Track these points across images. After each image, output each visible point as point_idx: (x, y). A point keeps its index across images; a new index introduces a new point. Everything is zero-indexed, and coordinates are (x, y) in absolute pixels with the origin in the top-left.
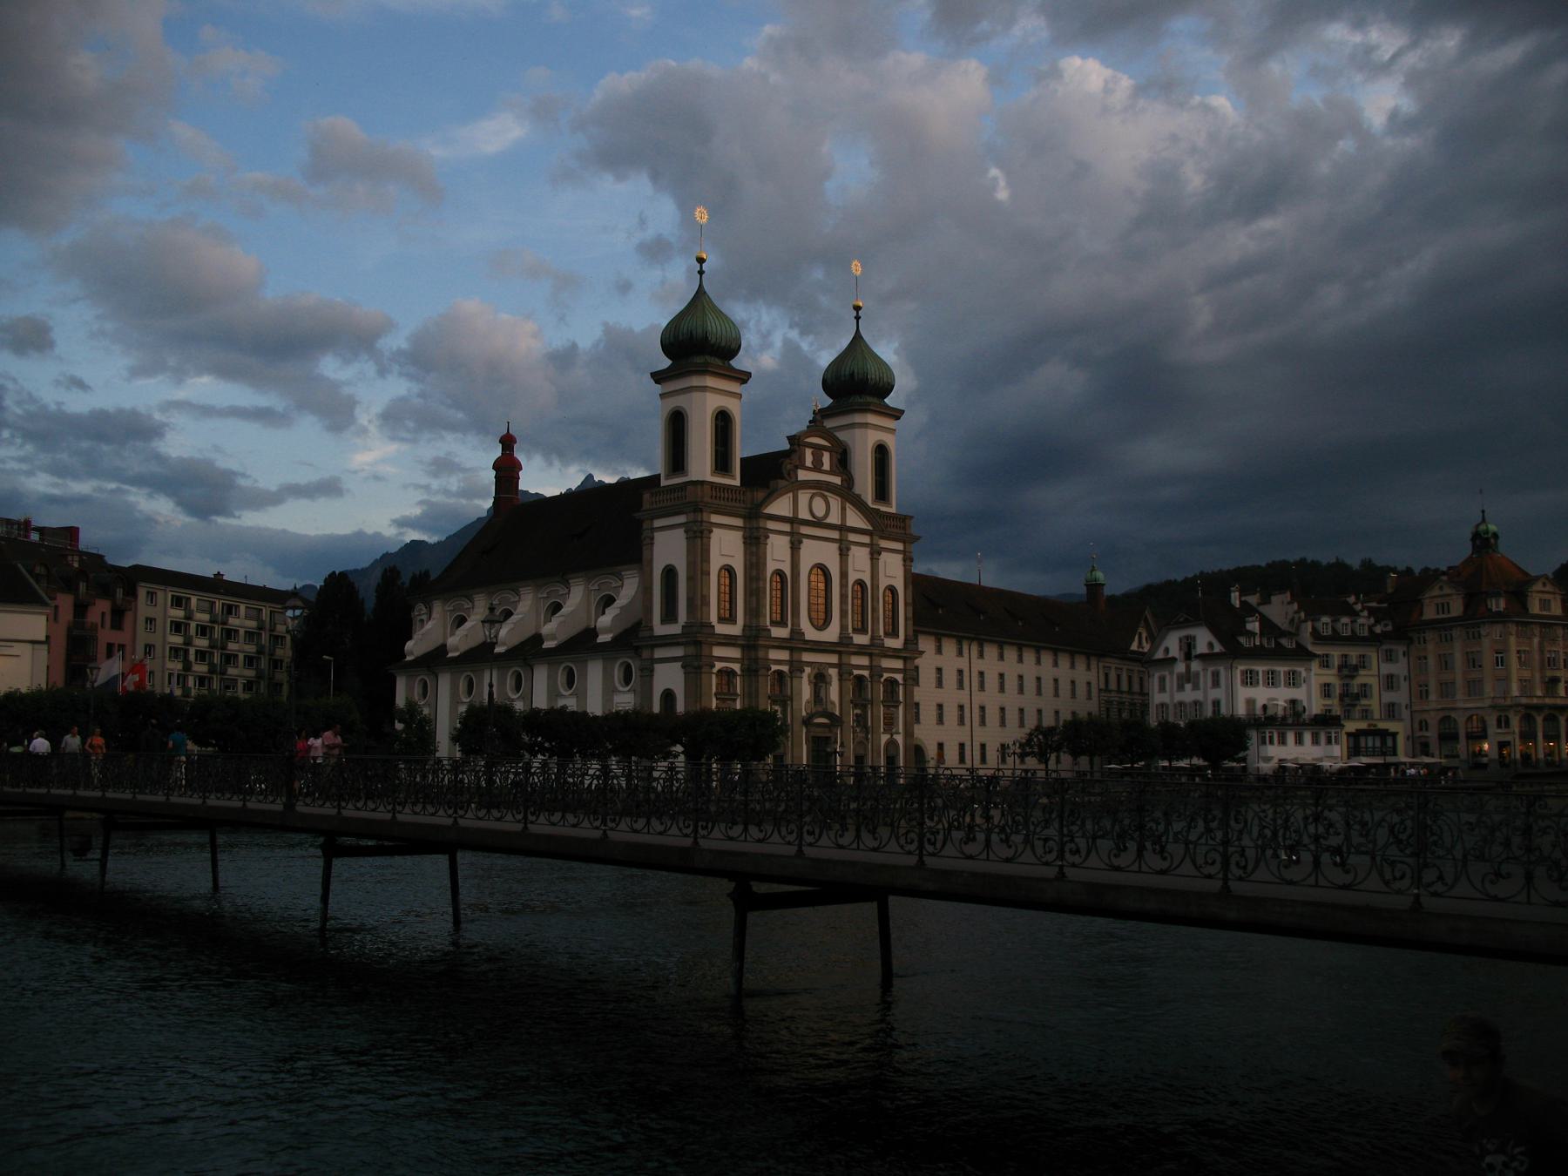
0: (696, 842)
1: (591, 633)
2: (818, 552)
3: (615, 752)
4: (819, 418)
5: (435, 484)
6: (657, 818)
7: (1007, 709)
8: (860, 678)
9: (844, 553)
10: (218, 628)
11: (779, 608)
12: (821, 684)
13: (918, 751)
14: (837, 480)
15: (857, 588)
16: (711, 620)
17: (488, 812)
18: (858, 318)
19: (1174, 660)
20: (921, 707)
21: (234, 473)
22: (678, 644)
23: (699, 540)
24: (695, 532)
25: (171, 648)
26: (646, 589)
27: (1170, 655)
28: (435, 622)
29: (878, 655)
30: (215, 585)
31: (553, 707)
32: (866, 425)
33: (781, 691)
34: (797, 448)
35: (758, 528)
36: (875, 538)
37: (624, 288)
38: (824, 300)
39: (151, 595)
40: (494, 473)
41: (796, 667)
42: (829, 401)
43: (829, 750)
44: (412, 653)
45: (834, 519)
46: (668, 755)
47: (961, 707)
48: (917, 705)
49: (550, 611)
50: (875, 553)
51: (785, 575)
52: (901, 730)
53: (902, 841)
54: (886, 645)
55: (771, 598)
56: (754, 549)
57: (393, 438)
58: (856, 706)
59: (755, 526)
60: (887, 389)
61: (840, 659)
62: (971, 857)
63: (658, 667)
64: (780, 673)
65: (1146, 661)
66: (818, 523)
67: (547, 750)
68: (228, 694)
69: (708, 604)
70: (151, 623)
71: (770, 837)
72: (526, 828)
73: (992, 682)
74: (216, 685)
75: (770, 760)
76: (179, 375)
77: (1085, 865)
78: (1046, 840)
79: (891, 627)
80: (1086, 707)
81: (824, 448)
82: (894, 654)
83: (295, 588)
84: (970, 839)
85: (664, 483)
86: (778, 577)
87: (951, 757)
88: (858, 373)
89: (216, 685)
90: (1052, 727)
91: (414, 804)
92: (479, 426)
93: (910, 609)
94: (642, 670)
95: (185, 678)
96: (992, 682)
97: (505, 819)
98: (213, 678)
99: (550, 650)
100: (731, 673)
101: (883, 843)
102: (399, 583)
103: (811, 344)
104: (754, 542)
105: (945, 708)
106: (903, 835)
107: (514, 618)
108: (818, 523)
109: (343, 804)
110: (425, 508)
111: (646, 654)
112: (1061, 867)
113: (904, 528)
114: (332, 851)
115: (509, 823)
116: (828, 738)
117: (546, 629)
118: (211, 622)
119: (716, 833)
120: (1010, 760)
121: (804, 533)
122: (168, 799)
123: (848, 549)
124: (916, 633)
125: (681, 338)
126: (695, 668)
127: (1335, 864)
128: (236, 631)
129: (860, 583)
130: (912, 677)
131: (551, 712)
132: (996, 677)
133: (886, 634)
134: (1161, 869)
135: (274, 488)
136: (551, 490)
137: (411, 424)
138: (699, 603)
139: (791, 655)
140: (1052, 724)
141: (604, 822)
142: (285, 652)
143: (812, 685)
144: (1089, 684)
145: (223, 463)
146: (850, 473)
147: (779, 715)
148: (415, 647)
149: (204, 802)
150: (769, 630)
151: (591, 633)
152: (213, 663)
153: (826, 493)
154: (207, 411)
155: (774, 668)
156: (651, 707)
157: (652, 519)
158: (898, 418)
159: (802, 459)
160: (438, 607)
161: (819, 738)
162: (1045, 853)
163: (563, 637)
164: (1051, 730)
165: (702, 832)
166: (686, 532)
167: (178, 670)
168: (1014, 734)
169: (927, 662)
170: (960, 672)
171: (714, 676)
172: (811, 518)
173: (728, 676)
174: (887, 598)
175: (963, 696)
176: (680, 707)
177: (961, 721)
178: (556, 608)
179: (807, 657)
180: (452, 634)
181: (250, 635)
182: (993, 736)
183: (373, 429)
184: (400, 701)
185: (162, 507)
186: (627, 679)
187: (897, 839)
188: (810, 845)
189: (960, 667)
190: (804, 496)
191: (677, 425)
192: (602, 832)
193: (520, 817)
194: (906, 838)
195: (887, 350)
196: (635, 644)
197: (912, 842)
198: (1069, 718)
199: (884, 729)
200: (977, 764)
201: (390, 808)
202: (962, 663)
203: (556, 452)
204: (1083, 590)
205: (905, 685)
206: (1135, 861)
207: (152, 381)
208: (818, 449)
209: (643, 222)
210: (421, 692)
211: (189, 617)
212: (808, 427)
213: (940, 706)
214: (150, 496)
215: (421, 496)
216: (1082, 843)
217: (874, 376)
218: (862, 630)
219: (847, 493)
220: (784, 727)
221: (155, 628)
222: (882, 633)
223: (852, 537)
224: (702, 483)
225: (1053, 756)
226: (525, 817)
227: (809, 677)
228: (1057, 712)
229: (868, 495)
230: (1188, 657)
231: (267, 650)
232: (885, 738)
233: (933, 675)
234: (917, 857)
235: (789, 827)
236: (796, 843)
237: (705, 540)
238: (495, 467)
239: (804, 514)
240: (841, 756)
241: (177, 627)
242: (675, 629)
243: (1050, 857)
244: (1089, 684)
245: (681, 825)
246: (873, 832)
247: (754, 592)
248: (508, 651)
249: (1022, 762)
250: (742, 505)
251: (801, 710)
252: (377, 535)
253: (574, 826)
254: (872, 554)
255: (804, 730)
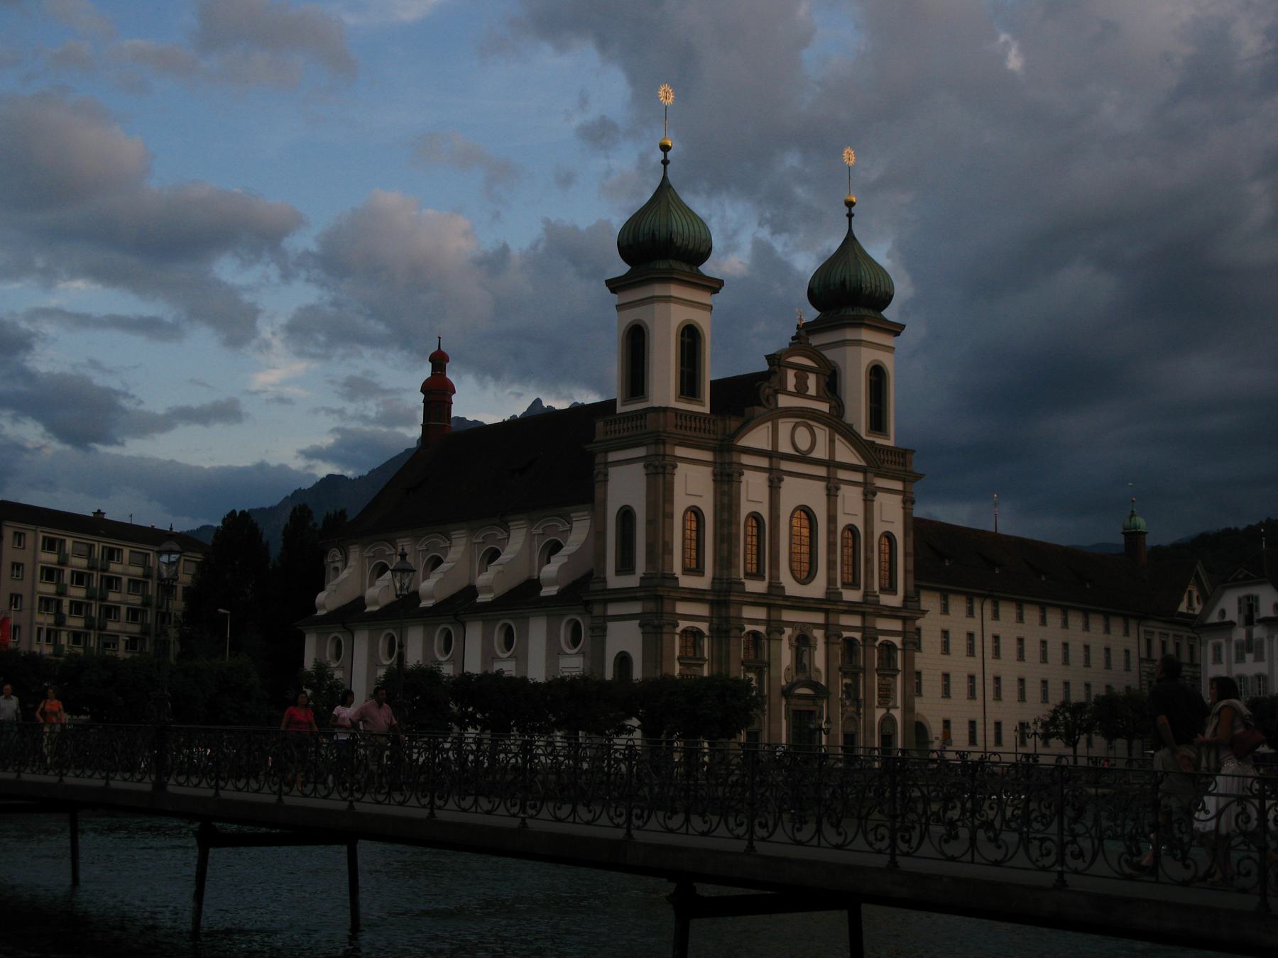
0: (629, 834)
1: (533, 585)
2: (810, 493)
3: (558, 726)
4: (803, 333)
5: (351, 408)
6: (584, 805)
7: (1026, 680)
8: (850, 641)
9: (832, 494)
10: (96, 576)
11: (754, 557)
12: (803, 649)
13: (920, 730)
14: (824, 407)
15: (885, 541)
16: (675, 571)
17: (188, 779)
18: (850, 216)
19: (1231, 624)
20: (924, 677)
21: (116, 393)
22: (635, 599)
23: (661, 476)
24: (656, 467)
25: (41, 599)
26: (599, 534)
27: (1227, 619)
28: (351, 570)
29: (870, 614)
30: (95, 525)
31: (486, 672)
32: (859, 343)
33: (756, 657)
34: (777, 369)
35: (731, 463)
36: (870, 475)
37: (566, 180)
38: (800, 192)
39: (19, 536)
40: (422, 396)
41: (775, 627)
42: (626, 268)
43: (812, 726)
44: (323, 607)
45: (821, 453)
46: (622, 730)
47: (972, 678)
48: (919, 674)
49: (486, 560)
50: (869, 494)
51: (858, 531)
52: (899, 704)
53: (871, 837)
54: (881, 603)
55: (746, 544)
56: (726, 488)
57: (300, 354)
58: (845, 675)
59: (661, 452)
60: (886, 300)
61: (827, 618)
62: (952, 859)
63: (611, 626)
64: (755, 635)
65: (1196, 625)
66: (802, 458)
67: (479, 722)
68: (107, 653)
69: (671, 552)
70: (18, 569)
71: (851, 842)
72: (432, 814)
73: (1009, 648)
74: (93, 642)
75: (742, 738)
76: (49, 277)
77: (915, 854)
78: (1042, 840)
79: (887, 581)
80: (1124, 679)
81: (811, 370)
82: (892, 613)
83: (171, 529)
84: (952, 836)
85: (620, 409)
86: (754, 522)
87: (960, 738)
88: (850, 281)
89: (93, 642)
90: (1082, 703)
91: (304, 784)
92: (403, 338)
93: (911, 560)
94: (592, 629)
95: (57, 633)
96: (1009, 648)
97: (598, 822)
98: (90, 634)
99: (486, 606)
100: (697, 634)
101: (848, 840)
102: (311, 524)
103: (785, 245)
104: (726, 479)
105: (952, 679)
106: (871, 830)
107: (444, 567)
108: (802, 458)
109: (222, 784)
110: (338, 437)
111: (597, 610)
112: (1061, 874)
113: (904, 465)
114: (209, 839)
115: (415, 809)
116: (812, 712)
117: (482, 580)
118: (89, 568)
119: (653, 824)
120: (1030, 742)
121: (785, 469)
122: (19, 776)
123: (838, 489)
124: (918, 589)
125: (641, 239)
126: (655, 627)
127: (989, 839)
128: (119, 579)
129: (851, 529)
130: (913, 641)
131: (485, 676)
132: (964, 637)
133: (882, 590)
134: (952, 856)
135: (161, 411)
136: (490, 418)
137: (321, 338)
138: (661, 550)
139: (769, 614)
140: (1082, 699)
141: (523, 809)
142: (177, 605)
143: (794, 649)
144: (1127, 652)
145: (100, 380)
146: (841, 399)
147: (754, 683)
148: (327, 600)
149: (61, 780)
150: (743, 584)
151: (533, 585)
152: (91, 617)
153: (811, 423)
154: (82, 321)
155: (748, 628)
156: (603, 674)
157: (607, 452)
158: (897, 334)
159: (783, 382)
160: (355, 554)
161: (800, 711)
162: (1042, 855)
163: (501, 590)
164: (1080, 707)
165: (636, 822)
166: (646, 467)
167: (48, 624)
168: (1035, 710)
169: (931, 622)
170: (971, 636)
171: (677, 638)
172: (793, 452)
173: (695, 637)
174: (883, 547)
175: (974, 665)
176: (637, 674)
177: (972, 694)
178: (494, 555)
179: (788, 616)
180: (372, 585)
181: (135, 584)
182: (1010, 712)
183: (277, 343)
184: (309, 664)
185: (30, 432)
186: (575, 640)
187: (865, 835)
188: (763, 839)
189: (971, 630)
190: (785, 426)
191: (636, 340)
192: (520, 820)
193: (425, 801)
194: (875, 835)
195: (880, 251)
196: (585, 599)
197: (883, 838)
198: (1103, 692)
199: (879, 702)
200: (991, 746)
201: (276, 788)
202: (974, 625)
203: (490, 370)
204: (1121, 540)
205: (904, 650)
206: (967, 851)
207: (16, 286)
208: (802, 371)
209: (584, 102)
210: (334, 651)
211: (63, 562)
212: (790, 344)
213: (946, 676)
214: (15, 420)
215: (333, 422)
216: (1086, 844)
217: (869, 285)
218: (854, 585)
219: (837, 423)
220: (759, 699)
221: (22, 576)
222: (876, 588)
223: (842, 475)
224: (666, 409)
225: (1083, 739)
226: (432, 802)
227: (790, 639)
228: (1088, 686)
229: (862, 428)
230: (1249, 621)
231: (154, 601)
232: (879, 713)
233: (938, 640)
234: (746, 843)
235: (618, 810)
236: (747, 837)
237: (668, 477)
238: (422, 391)
239: (785, 447)
240: (827, 733)
241: (49, 574)
242: (632, 581)
243: (1047, 861)
244: (1127, 652)
245: (612, 814)
246: (836, 826)
247: (725, 538)
248: (436, 606)
249: (1046, 744)
250: (713, 436)
251: (780, 678)
252: (282, 468)
253: (489, 813)
254: (865, 494)
255: (784, 702)
